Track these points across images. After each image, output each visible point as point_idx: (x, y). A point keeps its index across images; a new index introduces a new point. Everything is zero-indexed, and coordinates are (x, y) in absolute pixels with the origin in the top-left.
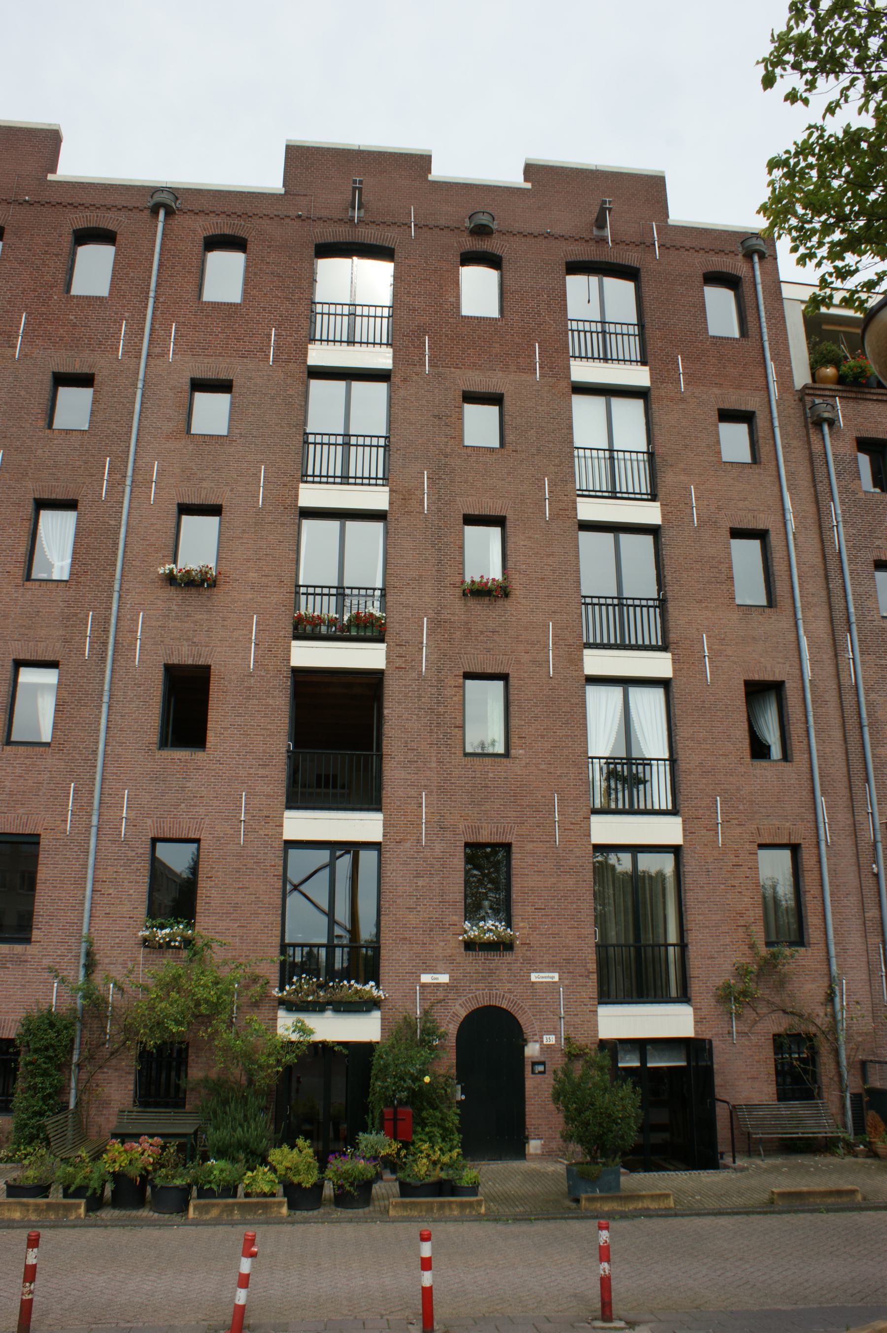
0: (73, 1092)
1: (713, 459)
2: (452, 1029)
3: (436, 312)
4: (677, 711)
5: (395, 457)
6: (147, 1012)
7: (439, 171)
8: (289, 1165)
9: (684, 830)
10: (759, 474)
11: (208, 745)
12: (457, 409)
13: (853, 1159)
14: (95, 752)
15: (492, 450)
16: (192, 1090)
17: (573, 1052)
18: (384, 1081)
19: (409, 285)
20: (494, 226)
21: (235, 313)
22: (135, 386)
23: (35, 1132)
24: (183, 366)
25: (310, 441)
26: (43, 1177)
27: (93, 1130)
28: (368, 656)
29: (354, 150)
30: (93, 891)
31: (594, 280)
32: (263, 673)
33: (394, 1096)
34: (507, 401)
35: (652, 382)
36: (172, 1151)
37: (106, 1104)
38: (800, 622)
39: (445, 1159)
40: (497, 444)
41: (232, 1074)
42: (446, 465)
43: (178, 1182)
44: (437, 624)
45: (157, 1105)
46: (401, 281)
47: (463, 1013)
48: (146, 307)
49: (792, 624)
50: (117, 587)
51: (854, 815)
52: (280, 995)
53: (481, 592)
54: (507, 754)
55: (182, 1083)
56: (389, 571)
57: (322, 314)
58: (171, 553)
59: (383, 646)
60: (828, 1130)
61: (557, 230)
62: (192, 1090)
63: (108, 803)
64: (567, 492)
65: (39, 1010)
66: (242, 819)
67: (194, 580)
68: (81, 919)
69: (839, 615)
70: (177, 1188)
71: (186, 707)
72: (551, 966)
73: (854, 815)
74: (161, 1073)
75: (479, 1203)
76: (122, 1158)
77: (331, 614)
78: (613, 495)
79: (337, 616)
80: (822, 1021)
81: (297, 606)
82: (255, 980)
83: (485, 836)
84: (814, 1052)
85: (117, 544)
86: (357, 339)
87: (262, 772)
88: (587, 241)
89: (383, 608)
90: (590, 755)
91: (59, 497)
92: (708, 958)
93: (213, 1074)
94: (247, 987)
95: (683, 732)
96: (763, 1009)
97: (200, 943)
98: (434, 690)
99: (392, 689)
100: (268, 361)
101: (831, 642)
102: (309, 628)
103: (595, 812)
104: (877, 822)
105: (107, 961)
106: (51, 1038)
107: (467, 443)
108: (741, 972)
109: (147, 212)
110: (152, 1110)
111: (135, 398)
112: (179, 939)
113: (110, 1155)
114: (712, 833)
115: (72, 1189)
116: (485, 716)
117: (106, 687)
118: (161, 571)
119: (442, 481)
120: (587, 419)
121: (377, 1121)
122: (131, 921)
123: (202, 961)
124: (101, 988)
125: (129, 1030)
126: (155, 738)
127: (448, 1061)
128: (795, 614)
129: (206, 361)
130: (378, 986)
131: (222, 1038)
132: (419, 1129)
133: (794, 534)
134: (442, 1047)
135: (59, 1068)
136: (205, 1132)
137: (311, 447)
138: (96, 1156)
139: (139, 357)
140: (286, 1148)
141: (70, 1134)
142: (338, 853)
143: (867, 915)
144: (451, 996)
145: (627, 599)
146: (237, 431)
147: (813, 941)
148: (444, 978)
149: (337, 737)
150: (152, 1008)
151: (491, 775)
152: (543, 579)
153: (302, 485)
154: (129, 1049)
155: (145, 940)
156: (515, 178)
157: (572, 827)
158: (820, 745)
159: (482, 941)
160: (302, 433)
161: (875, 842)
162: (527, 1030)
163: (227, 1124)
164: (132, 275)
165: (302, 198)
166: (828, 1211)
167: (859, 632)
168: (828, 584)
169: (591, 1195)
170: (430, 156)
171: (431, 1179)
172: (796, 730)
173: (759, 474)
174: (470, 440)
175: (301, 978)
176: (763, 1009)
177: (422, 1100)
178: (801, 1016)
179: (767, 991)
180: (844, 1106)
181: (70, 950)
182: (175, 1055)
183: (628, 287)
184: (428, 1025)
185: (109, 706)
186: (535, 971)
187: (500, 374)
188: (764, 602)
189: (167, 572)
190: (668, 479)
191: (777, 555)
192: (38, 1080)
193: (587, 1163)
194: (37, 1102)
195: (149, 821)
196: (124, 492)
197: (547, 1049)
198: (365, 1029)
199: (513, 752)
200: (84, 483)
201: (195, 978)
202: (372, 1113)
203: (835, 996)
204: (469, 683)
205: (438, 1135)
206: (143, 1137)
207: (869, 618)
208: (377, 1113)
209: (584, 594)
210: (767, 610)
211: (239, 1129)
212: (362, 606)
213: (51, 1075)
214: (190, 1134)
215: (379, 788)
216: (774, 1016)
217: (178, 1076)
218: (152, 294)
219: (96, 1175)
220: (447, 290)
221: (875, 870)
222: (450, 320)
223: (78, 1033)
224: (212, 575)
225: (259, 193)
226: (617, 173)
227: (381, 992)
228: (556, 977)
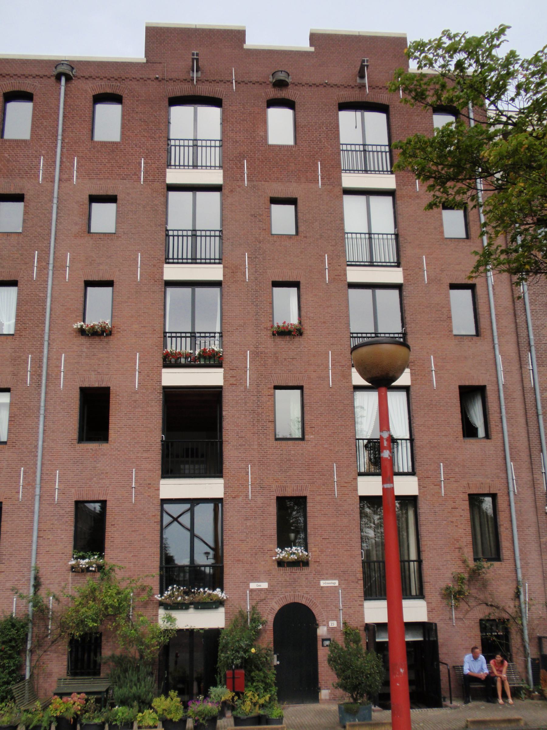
0: (28, 669)
1: (438, 237)
2: (270, 618)
3: (251, 143)
4: (413, 407)
5: (226, 244)
6: (74, 614)
7: (252, 41)
9: (419, 485)
10: (470, 246)
11: (110, 439)
12: (266, 210)
14: (36, 447)
15: (289, 236)
16: (105, 663)
18: (226, 653)
19: (233, 124)
20: (289, 80)
21: (117, 148)
22: (51, 201)
23: (4, 694)
24: (81, 185)
25: (170, 234)
26: (13, 720)
27: (41, 693)
28: (211, 377)
29: (192, 29)
30: (38, 537)
31: (359, 114)
32: (144, 391)
33: (233, 662)
34: (299, 202)
36: (92, 702)
37: (50, 675)
38: (497, 346)
40: (294, 232)
41: (130, 652)
42: (260, 248)
43: (96, 721)
44: (256, 355)
45: (82, 674)
46: (227, 121)
47: (277, 608)
48: (56, 147)
49: (492, 347)
50: (46, 338)
51: (533, 474)
52: (160, 599)
53: (284, 333)
55: (98, 659)
56: (224, 321)
57: (175, 146)
58: (81, 314)
59: (221, 370)
60: (515, 682)
61: (334, 80)
62: (105, 663)
63: (47, 479)
64: (341, 262)
65: (5, 616)
66: (133, 486)
67: (97, 332)
68: (30, 556)
69: (523, 340)
70: (96, 724)
71: (95, 414)
72: (332, 576)
73: (533, 474)
74: (84, 654)
76: (62, 707)
77: (187, 351)
78: (371, 264)
79: (192, 351)
81: (165, 346)
82: (143, 589)
85: (44, 309)
87: (145, 455)
89: (222, 345)
90: (357, 437)
91: (5, 279)
92: (436, 569)
93: (118, 652)
94: (138, 595)
96: (472, 603)
97: (107, 568)
98: (255, 398)
99: (228, 398)
100: (140, 181)
101: (518, 358)
102: (173, 360)
103: (360, 474)
105: (48, 582)
106: (14, 634)
109: (53, 79)
110: (80, 677)
111: (52, 210)
112: (94, 565)
113: (54, 705)
115: (31, 727)
116: (288, 409)
117: (42, 404)
118: (75, 327)
119: (257, 260)
121: (223, 679)
122: (63, 555)
123: (109, 579)
124: (45, 600)
125: (63, 626)
126: (76, 436)
127: (267, 639)
128: (493, 340)
129: (98, 183)
130: (222, 591)
131: (122, 630)
132: (249, 684)
133: (493, 286)
135: (19, 653)
136: (113, 689)
137: (171, 238)
138: (45, 708)
139: (53, 181)
141: (27, 695)
143: (542, 540)
144: (269, 597)
145: (380, 334)
146: (122, 230)
147: (505, 557)
148: (265, 585)
149: (193, 430)
150: (77, 611)
151: (293, 452)
152: (324, 322)
154: (63, 638)
155: (72, 567)
156: (303, 44)
157: (346, 485)
158: (509, 427)
159: (288, 560)
160: (165, 230)
162: (319, 618)
163: (127, 684)
164: (45, 124)
165: (158, 65)
167: (537, 351)
168: (516, 320)
173: (470, 246)
175: (173, 588)
176: (472, 603)
177: (250, 665)
178: (498, 607)
180: (526, 667)
181: (24, 577)
182: (93, 641)
183: (381, 117)
184: (255, 616)
185: (45, 417)
186: (323, 579)
187: (295, 185)
189: (79, 327)
190: (408, 251)
191: (481, 301)
192: (6, 661)
194: (5, 675)
195: (73, 490)
196: (48, 274)
197: (331, 630)
199: (306, 437)
200: (21, 269)
201: (104, 591)
202: (220, 674)
203: (520, 594)
204: (277, 391)
205: (262, 687)
206: (73, 694)
208: (222, 675)
209: (352, 331)
210: (475, 338)
211: (134, 688)
212: (207, 344)
213: (13, 658)
214: (104, 692)
216: (479, 608)
217: (96, 655)
218: (60, 137)
219: (46, 719)
220: (258, 127)
222: (261, 148)
223: (30, 630)
224: (108, 328)
225: (129, 63)
226: (374, 36)
227: (223, 594)
228: (336, 583)
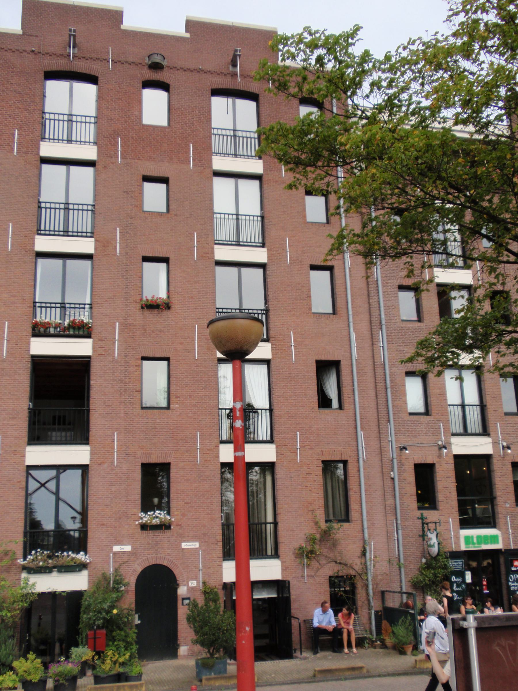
2: (131, 579)
4: (273, 379)
7: (129, 23)
8: (25, 669)
9: (277, 452)
13: (373, 650)
15: (160, 214)
17: (207, 591)
20: (165, 63)
32: (12, 359)
33: (94, 623)
34: (171, 181)
35: (264, 170)
38: (351, 324)
39: (121, 660)
40: (165, 210)
44: (124, 327)
47: (139, 569)
53: (153, 306)
54: (168, 408)
56: (94, 293)
59: (90, 341)
64: (209, 241)
69: (375, 319)
75: (141, 685)
78: (238, 243)
80: (358, 567)
81: (35, 315)
83: (153, 459)
84: (353, 586)
86: (74, 138)
88: (225, 75)
89: (91, 316)
90: (220, 407)
95: (276, 393)
96: (323, 561)
98: (123, 368)
102: (42, 330)
103: (222, 442)
104: (394, 446)
107: (145, 209)
108: (312, 540)
114: (294, 454)
116: (155, 379)
120: (222, 192)
121: (84, 640)
127: (129, 600)
128: (348, 319)
132: (111, 643)
133: (350, 269)
134: (127, 591)
140: (22, 660)
142: (61, 471)
144: (132, 559)
147: (354, 519)
148: (128, 548)
151: (158, 421)
152: (192, 297)
153: (37, 237)
156: (179, 30)
157: (208, 452)
161: (393, 459)
162: (179, 578)
166: (346, 679)
167: (387, 329)
168: (369, 300)
169: (208, 677)
170: (122, 12)
171: (113, 672)
172: (346, 391)
174: (147, 207)
176: (323, 561)
177: (112, 625)
178: (346, 565)
179: (326, 550)
180: (370, 619)
183: (252, 105)
186: (184, 541)
188: (331, 311)
190: (272, 233)
191: (338, 281)
193: (208, 658)
197: (191, 590)
198: (77, 582)
204: (145, 362)
207: (393, 321)
208: (84, 635)
209: (218, 307)
210: (332, 316)
212: (77, 314)
215: (87, 430)
220: (133, 107)
221: (392, 476)
228: (196, 545)
